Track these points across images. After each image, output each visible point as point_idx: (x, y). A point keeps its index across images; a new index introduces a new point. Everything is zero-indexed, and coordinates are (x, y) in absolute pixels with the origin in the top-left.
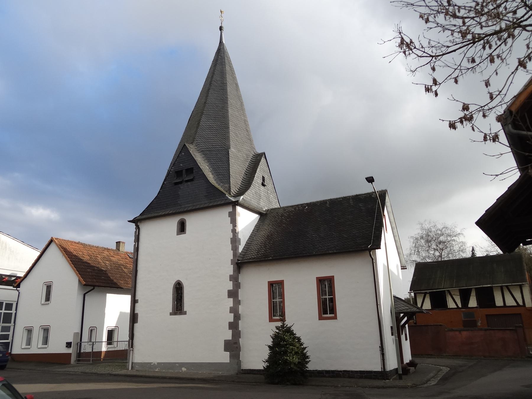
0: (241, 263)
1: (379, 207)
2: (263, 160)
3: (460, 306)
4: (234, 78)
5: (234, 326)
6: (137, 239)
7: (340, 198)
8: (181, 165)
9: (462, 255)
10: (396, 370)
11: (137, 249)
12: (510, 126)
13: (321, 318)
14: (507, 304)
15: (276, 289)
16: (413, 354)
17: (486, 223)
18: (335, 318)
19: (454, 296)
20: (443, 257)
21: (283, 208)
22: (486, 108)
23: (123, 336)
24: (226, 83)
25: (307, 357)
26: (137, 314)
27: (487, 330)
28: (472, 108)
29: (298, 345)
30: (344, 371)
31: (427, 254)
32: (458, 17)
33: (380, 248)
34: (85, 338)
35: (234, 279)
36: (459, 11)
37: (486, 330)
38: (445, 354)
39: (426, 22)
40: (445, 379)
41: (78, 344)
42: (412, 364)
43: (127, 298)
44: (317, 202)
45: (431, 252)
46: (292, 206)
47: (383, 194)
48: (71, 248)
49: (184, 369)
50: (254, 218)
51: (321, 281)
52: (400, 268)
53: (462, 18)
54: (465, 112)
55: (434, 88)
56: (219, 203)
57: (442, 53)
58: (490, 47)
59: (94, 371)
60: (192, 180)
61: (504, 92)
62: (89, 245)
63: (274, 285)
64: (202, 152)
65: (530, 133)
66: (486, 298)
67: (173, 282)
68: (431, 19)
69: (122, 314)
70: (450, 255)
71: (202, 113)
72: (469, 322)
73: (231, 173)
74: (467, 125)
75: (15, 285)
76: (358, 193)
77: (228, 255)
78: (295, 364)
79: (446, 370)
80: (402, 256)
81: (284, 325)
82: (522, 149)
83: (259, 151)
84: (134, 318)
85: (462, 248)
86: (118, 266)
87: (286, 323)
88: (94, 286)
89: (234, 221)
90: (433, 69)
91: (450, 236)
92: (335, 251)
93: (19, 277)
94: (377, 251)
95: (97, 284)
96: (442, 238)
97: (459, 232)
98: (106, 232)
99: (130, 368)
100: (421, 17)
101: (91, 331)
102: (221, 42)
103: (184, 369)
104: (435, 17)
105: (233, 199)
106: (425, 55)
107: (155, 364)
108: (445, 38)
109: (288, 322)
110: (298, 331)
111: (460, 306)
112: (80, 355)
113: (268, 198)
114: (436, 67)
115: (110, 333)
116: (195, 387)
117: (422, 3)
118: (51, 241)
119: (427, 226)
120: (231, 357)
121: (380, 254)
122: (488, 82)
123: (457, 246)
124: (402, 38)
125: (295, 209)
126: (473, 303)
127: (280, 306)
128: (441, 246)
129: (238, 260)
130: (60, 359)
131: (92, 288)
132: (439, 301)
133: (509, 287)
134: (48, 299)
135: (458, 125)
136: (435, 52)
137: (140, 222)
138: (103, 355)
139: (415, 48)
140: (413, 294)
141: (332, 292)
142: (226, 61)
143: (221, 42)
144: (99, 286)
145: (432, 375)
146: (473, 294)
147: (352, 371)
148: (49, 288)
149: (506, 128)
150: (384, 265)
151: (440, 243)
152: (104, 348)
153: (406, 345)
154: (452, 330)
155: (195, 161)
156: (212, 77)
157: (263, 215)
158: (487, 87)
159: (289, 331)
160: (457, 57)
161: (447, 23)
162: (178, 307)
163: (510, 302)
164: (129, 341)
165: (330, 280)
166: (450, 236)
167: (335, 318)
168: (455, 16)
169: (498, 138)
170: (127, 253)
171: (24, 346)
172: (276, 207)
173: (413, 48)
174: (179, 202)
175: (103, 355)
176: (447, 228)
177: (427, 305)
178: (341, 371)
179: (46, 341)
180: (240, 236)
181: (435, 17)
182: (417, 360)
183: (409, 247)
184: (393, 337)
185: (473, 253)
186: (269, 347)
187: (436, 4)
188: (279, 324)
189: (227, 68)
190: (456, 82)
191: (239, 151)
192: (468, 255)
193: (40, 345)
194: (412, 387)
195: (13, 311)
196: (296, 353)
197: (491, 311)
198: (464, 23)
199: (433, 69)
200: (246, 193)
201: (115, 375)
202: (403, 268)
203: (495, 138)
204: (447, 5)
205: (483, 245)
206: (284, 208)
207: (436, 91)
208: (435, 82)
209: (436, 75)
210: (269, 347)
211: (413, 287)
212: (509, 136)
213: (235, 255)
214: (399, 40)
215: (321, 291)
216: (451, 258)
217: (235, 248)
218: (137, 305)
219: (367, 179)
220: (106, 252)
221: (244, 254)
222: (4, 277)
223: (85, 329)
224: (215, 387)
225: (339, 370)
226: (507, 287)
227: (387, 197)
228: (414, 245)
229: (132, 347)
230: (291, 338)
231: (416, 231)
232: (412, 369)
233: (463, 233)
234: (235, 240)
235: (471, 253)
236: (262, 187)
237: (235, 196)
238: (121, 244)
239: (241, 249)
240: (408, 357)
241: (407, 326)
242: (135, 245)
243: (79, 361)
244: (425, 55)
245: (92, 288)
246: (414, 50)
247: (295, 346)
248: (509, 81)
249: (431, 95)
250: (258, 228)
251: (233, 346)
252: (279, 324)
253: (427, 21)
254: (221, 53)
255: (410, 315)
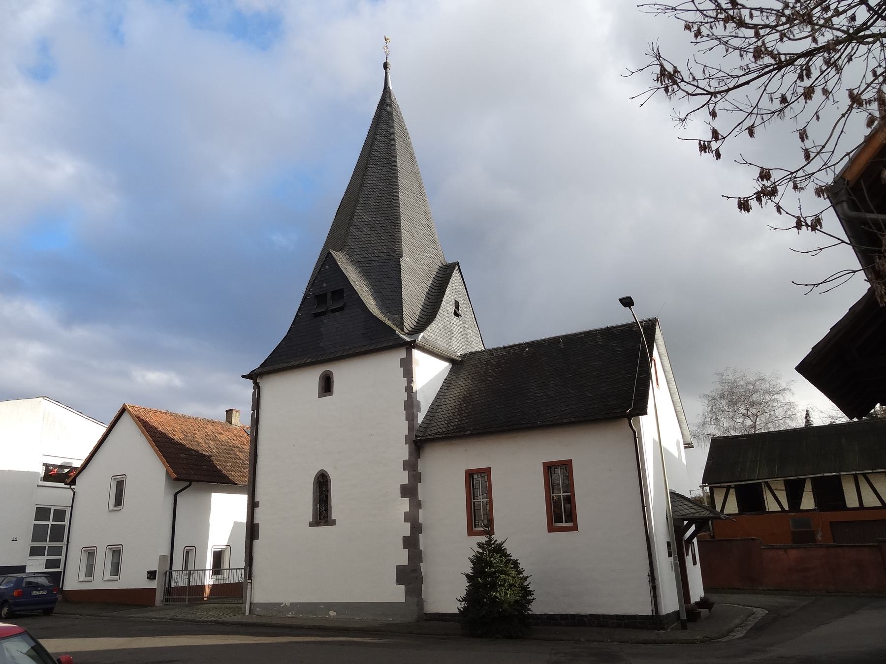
0: (421, 441)
1: (644, 347)
2: (456, 274)
3: (786, 508)
4: (408, 145)
5: (411, 543)
6: (256, 405)
7: (581, 333)
8: (325, 285)
9: (790, 424)
10: (677, 613)
11: (256, 421)
12: (845, 205)
13: (551, 529)
14: (866, 505)
15: (477, 482)
16: (706, 589)
17: (818, 368)
18: (575, 528)
19: (776, 492)
20: (758, 427)
21: (490, 350)
22: (800, 173)
23: (237, 559)
24: (395, 153)
25: (530, 593)
26: (258, 525)
27: (831, 546)
28: (776, 176)
29: (514, 573)
30: (590, 615)
31: (732, 424)
32: (747, 26)
33: (646, 414)
34: (178, 564)
35: (411, 466)
36: (751, 16)
37: (828, 547)
38: (760, 588)
39: (696, 36)
40: (759, 628)
41: (166, 574)
42: (704, 603)
43: (240, 501)
44: (544, 340)
45: (738, 420)
46: (504, 348)
47: (650, 326)
48: (154, 421)
49: (332, 613)
50: (443, 367)
51: (549, 468)
52: (682, 446)
53: (755, 27)
54: (765, 182)
55: (714, 145)
56: (384, 345)
57: (726, 88)
58: (808, 76)
59: (190, 617)
60: (341, 309)
61: (829, 147)
62: (184, 416)
63: (475, 476)
64: (358, 264)
65: (881, 217)
66: (830, 494)
67: (314, 473)
68: (705, 30)
69: (236, 525)
70: (770, 425)
71: (357, 202)
72: (803, 535)
73: (404, 297)
74: (769, 204)
75: (68, 481)
76: (610, 325)
77: (399, 428)
78: (509, 603)
79: (761, 613)
80: (685, 426)
81: (491, 540)
82: (864, 239)
83: (450, 261)
84: (252, 531)
85: (789, 413)
86: (229, 449)
87: (498, 537)
88: (191, 482)
89: (408, 374)
90: (714, 114)
91: (768, 393)
92: (573, 420)
93: (75, 468)
94: (642, 418)
95: (196, 478)
96: (755, 397)
97: (784, 386)
98: (205, 394)
99: (247, 613)
100: (688, 27)
101: (188, 552)
102: (386, 89)
103: (332, 613)
104: (711, 28)
105: (408, 339)
106: (699, 91)
107: (286, 605)
108: (733, 63)
109: (498, 537)
110: (513, 550)
111: (786, 508)
112: (169, 591)
113: (465, 336)
114: (717, 111)
115: (218, 556)
116: (376, 644)
117: (691, 6)
118: (123, 410)
119: (730, 378)
120: (408, 593)
121: (646, 422)
122: (805, 131)
123: (781, 410)
124: (662, 65)
125: (508, 352)
126: (808, 502)
127: (485, 509)
128: (754, 411)
129: (417, 436)
130: (136, 599)
131: (188, 483)
132: (751, 500)
133: (869, 476)
134: (119, 502)
135: (753, 203)
136: (714, 85)
137: (261, 378)
138: (207, 592)
139: (682, 80)
140: (707, 489)
141: (569, 486)
142: (395, 118)
143: (386, 89)
144: (198, 481)
145: (737, 621)
146: (808, 486)
147: (604, 616)
148: (120, 486)
149: (838, 207)
150: (654, 440)
151: (753, 404)
152: (209, 580)
153: (695, 574)
154: (773, 548)
155: (346, 279)
156: (373, 143)
157: (457, 364)
158: (803, 141)
159: (499, 550)
160: (752, 92)
161: (727, 33)
162: (322, 514)
163: (870, 500)
164: (245, 569)
165: (567, 465)
166: (768, 393)
167: (575, 528)
168: (741, 24)
169: (820, 224)
170: (243, 428)
171: (82, 578)
172: (479, 350)
173: (679, 81)
174: (321, 345)
175: (207, 592)
176: (763, 380)
177: (732, 507)
178: (585, 616)
179: (116, 569)
180: (419, 398)
181: (711, 28)
182: (714, 598)
183: (701, 412)
184: (672, 559)
185: (808, 421)
186: (467, 576)
187: (713, 6)
188: (483, 539)
189: (397, 128)
190: (751, 134)
191: (417, 261)
192: (800, 423)
193: (107, 576)
194: (702, 642)
195: (66, 523)
196: (511, 586)
197: (838, 516)
198: (757, 35)
199: (714, 114)
200: (429, 328)
201: (223, 623)
202: (688, 446)
203: (816, 224)
204: (729, 6)
205: (816, 408)
206: (490, 352)
207: (717, 150)
208: (716, 135)
209: (717, 124)
210: (467, 576)
211: (708, 478)
212: (848, 223)
213: (411, 428)
214: (657, 69)
215: (550, 486)
216: (772, 430)
217: (411, 417)
218: (257, 510)
219: (621, 300)
220: (210, 427)
221: (425, 425)
222: (51, 468)
223: (180, 550)
224: (319, 639)
225: (583, 613)
226: (864, 475)
227: (658, 331)
228: (709, 409)
229: (250, 578)
230: (502, 561)
231: (713, 388)
232: (704, 612)
233: (792, 388)
234: (411, 404)
235: (804, 420)
236: (455, 318)
237: (410, 334)
238: (234, 413)
239: (421, 418)
240: (697, 592)
241: (695, 540)
242: (253, 414)
243: (167, 600)
244: (699, 91)
245: (188, 483)
246: (682, 85)
247: (509, 575)
248: (838, 129)
249: (709, 156)
250: (448, 384)
251: (410, 576)
252: (483, 539)
253: (698, 33)
254: (386, 104)
255: (701, 524)
